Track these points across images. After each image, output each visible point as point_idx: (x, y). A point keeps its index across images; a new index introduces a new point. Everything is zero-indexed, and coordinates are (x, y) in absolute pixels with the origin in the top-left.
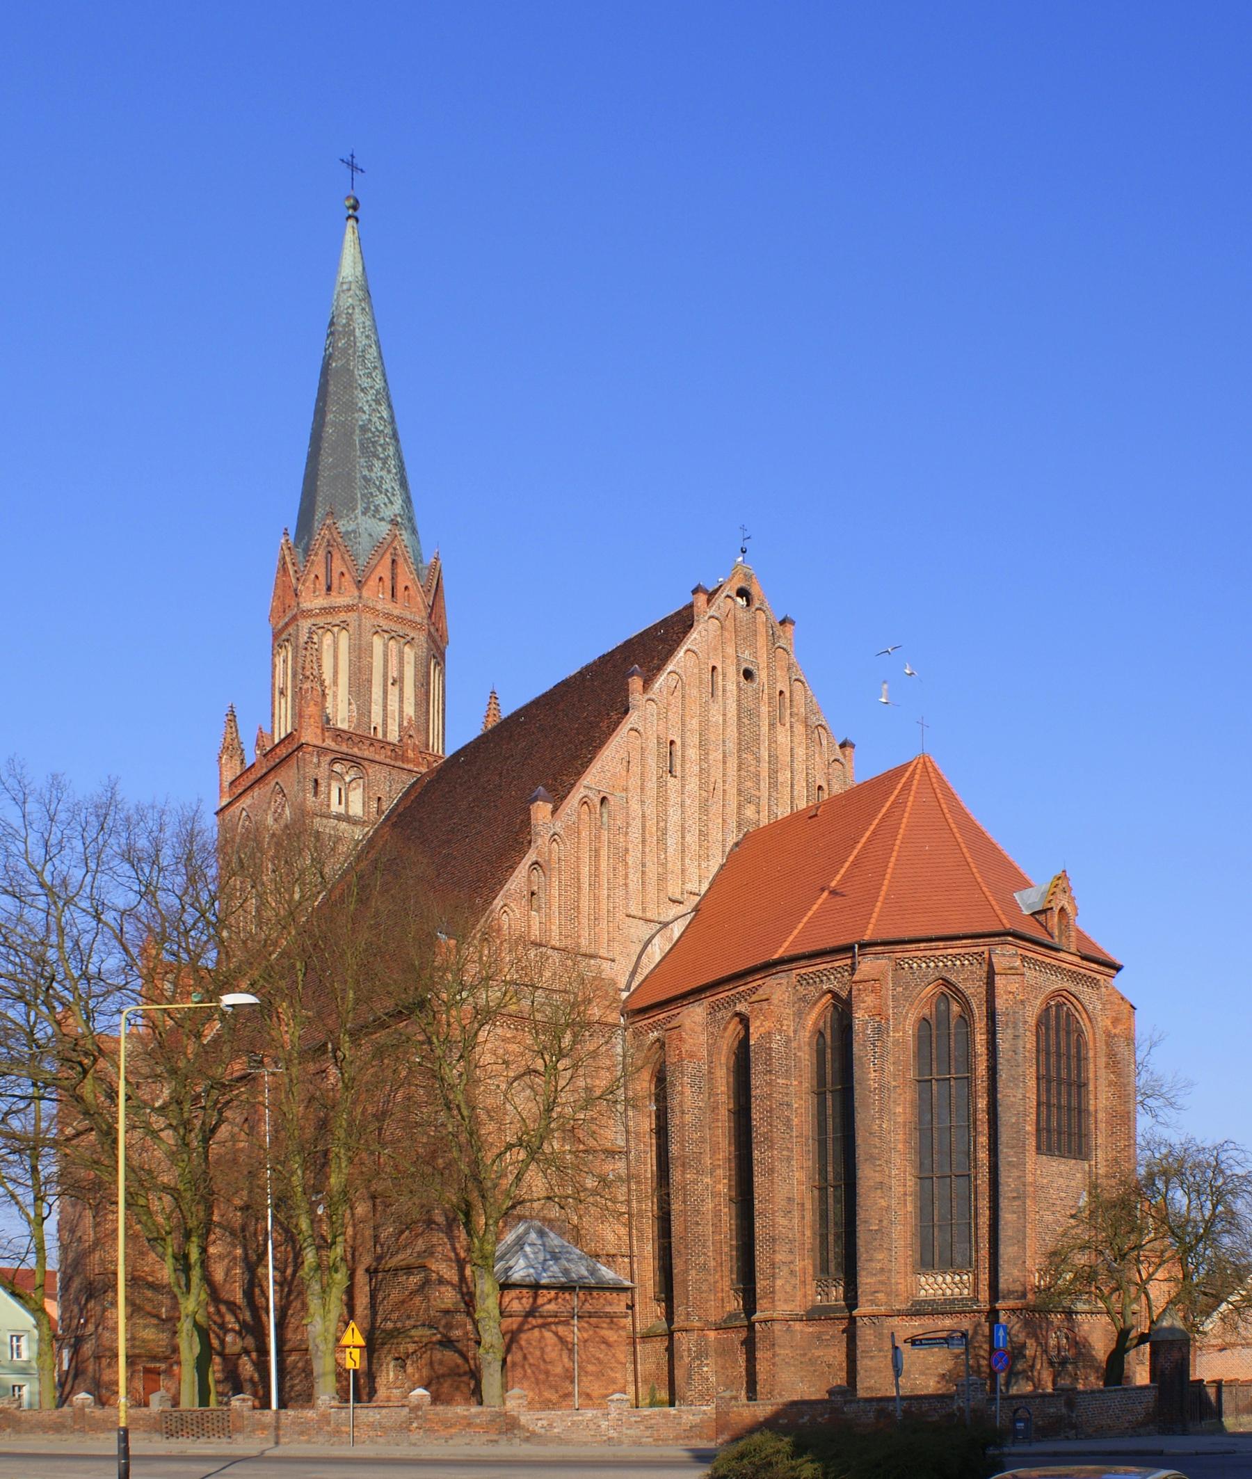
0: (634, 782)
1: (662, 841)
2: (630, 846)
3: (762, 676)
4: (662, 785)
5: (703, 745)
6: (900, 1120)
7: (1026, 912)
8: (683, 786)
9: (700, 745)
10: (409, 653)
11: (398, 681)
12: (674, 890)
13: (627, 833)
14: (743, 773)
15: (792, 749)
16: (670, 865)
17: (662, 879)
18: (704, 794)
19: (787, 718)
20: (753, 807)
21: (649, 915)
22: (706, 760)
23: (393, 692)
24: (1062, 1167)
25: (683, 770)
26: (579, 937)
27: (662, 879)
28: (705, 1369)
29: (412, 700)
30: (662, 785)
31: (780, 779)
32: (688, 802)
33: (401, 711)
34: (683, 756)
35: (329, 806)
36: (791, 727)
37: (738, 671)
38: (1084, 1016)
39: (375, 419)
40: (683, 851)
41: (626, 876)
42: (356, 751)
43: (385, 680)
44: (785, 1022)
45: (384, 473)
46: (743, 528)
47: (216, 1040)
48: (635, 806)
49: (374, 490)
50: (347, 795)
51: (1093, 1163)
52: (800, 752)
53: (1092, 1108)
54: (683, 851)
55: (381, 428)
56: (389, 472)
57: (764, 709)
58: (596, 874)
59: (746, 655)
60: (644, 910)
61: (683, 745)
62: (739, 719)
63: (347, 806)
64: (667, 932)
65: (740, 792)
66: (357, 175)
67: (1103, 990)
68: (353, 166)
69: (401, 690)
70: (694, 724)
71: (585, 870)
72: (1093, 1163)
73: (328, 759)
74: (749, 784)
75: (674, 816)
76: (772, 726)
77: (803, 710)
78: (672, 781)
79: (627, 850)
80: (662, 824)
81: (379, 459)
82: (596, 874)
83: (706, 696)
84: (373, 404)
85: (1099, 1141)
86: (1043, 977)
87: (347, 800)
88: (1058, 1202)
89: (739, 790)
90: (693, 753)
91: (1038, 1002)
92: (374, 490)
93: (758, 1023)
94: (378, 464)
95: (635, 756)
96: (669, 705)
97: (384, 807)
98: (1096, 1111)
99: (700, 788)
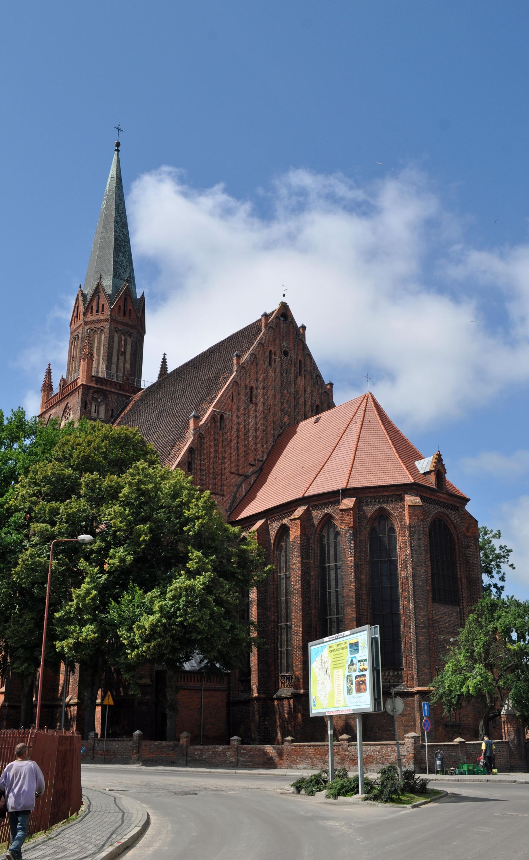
0: (235, 407)
1: (246, 435)
2: (233, 438)
3: (292, 353)
4: (247, 408)
5: (265, 388)
6: (364, 582)
7: (422, 472)
8: (256, 408)
9: (264, 388)
10: (129, 340)
11: (124, 353)
12: (251, 459)
13: (231, 432)
15: (305, 387)
17: (246, 454)
18: (266, 411)
19: (303, 372)
20: (287, 417)
21: (240, 472)
22: (267, 395)
23: (121, 359)
24: (446, 610)
25: (256, 400)
26: (209, 484)
27: (246, 454)
28: (266, 723)
29: (129, 362)
30: (247, 408)
31: (300, 402)
32: (258, 415)
33: (124, 367)
34: (256, 393)
35: (90, 414)
36: (305, 377)
37: (281, 352)
38: (452, 526)
39: (121, 235)
41: (230, 453)
42: (104, 387)
43: (118, 354)
44: (307, 530)
45: (123, 259)
46: (284, 285)
49: (119, 266)
50: (98, 408)
51: (461, 607)
52: (308, 389)
53: (459, 576)
54: (256, 440)
55: (123, 239)
56: (125, 258)
57: (292, 369)
59: (285, 344)
60: (238, 469)
61: (257, 388)
62: (282, 374)
63: (98, 414)
64: (248, 481)
65: (281, 410)
66: (121, 133)
68: (119, 130)
69: (125, 358)
70: (261, 378)
72: (461, 607)
73: (92, 391)
74: (285, 405)
75: (252, 423)
76: (296, 377)
77: (309, 368)
78: (252, 407)
79: (231, 440)
80: (247, 427)
81: (122, 252)
83: (267, 364)
85: (464, 595)
86: (431, 506)
87: (98, 410)
88: (445, 629)
89: (281, 409)
90: (260, 391)
91: (429, 519)
92: (119, 266)
93: (294, 530)
95: (235, 394)
96: (251, 369)
97: (114, 414)
98: (461, 578)
99: (264, 408)
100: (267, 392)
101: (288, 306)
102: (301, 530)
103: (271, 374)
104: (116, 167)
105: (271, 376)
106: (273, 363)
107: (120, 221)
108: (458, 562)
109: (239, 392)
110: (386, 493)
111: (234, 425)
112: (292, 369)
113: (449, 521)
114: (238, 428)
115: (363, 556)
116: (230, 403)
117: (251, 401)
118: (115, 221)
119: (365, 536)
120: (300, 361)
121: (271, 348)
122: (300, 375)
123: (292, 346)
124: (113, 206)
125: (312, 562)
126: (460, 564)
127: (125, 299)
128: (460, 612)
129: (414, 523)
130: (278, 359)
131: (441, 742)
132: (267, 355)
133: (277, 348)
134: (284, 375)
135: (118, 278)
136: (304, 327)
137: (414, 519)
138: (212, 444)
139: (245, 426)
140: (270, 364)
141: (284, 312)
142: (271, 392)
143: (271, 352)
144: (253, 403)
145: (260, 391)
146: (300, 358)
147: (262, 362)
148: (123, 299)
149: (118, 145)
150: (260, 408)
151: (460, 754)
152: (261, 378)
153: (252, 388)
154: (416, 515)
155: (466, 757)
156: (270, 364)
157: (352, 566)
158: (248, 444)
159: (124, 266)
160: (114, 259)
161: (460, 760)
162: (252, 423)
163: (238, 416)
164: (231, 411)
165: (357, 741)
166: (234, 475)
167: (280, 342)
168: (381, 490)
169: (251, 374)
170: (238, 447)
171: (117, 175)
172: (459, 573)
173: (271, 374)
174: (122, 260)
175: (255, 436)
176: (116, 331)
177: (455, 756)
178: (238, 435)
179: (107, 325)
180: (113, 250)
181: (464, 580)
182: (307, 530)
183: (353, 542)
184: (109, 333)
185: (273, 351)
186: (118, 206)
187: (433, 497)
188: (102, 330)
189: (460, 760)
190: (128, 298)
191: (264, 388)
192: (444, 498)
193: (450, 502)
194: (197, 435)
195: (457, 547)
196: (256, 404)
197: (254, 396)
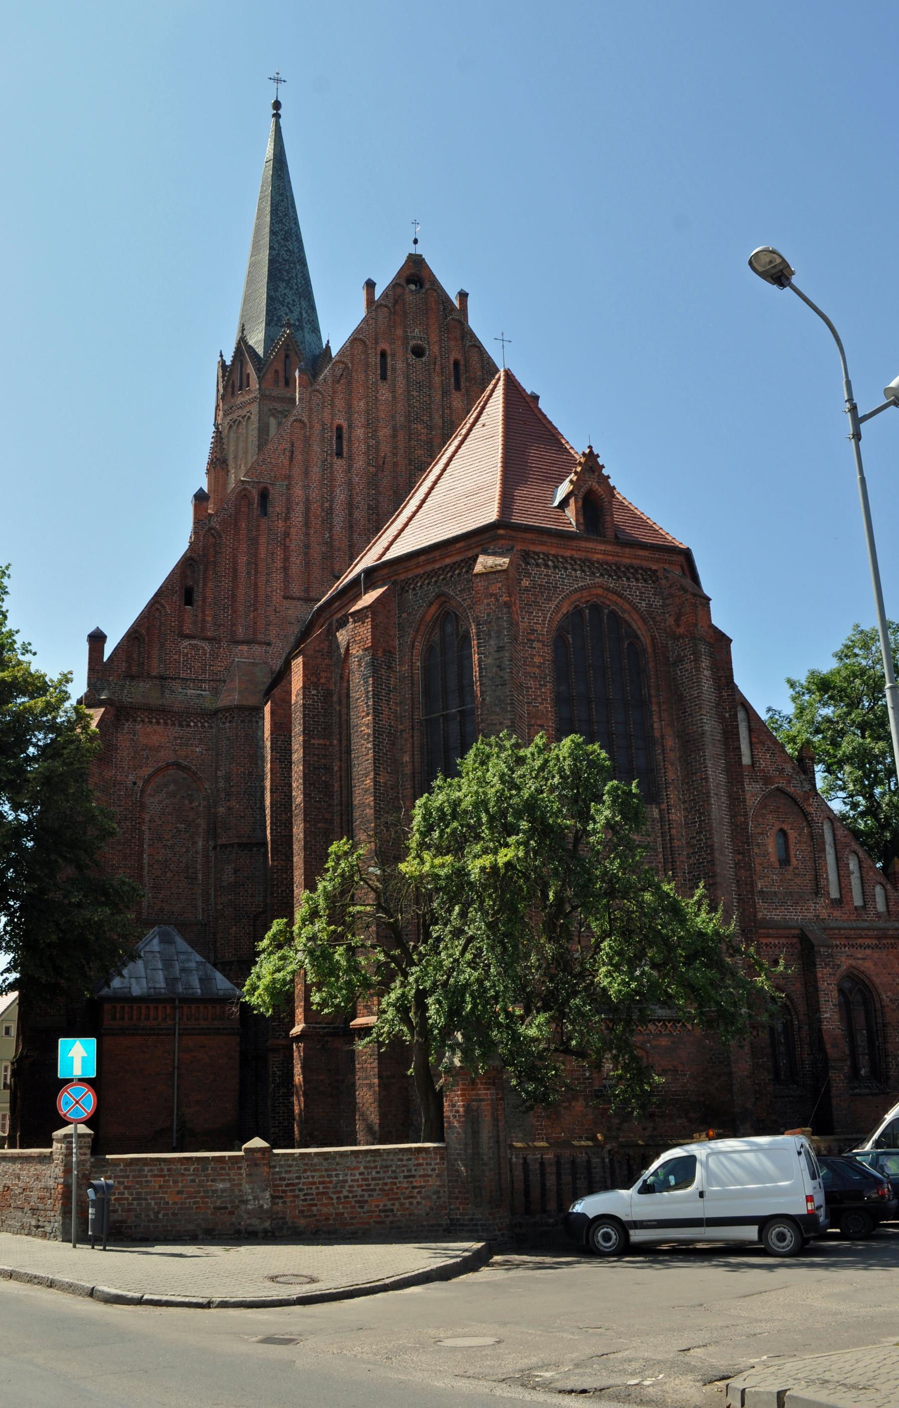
0: (297, 471)
14: (413, 443)
16: (336, 543)
25: (350, 450)
38: (636, 617)
40: (351, 527)
44: (323, 674)
47: (560, 899)
48: (298, 492)
49: (277, 305)
51: (664, 806)
53: (657, 734)
54: (351, 527)
57: (437, 379)
58: (254, 561)
61: (350, 426)
66: (281, 86)
67: (664, 581)
68: (278, 81)
70: (360, 405)
71: (243, 559)
75: (341, 496)
76: (445, 393)
77: (479, 373)
78: (339, 464)
81: (284, 281)
82: (254, 561)
84: (282, 242)
90: (359, 432)
92: (277, 305)
94: (282, 285)
95: (299, 444)
96: (334, 392)
98: (662, 737)
99: (369, 464)
100: (375, 431)
101: (424, 259)
102: (305, 675)
103: (384, 394)
104: (273, 144)
105: (386, 400)
106: (389, 373)
107: (281, 230)
108: (654, 700)
109: (307, 440)
110: (448, 561)
111: (298, 504)
112: (437, 379)
113: (626, 606)
114: (308, 509)
115: (405, 711)
116: (286, 462)
117: (339, 454)
118: (271, 231)
119: (410, 664)
120: (456, 363)
121: (383, 345)
122: (458, 387)
123: (434, 338)
124: (268, 209)
125: (335, 742)
126: (659, 704)
127: (287, 357)
128: (662, 819)
129: (488, 615)
130: (400, 365)
131: (331, 1145)
132: (375, 360)
133: (399, 343)
134: (415, 393)
135: (276, 325)
136: (463, 296)
137: (488, 605)
138: (244, 547)
139: (323, 504)
140: (384, 377)
141: (416, 273)
142: (384, 432)
143: (383, 354)
144: (342, 458)
145: (359, 432)
146: (455, 355)
147: (362, 377)
148: (282, 357)
149: (277, 105)
150: (360, 463)
151: (246, 1187)
152: (360, 405)
153: (339, 429)
154: (492, 595)
155: (267, 1195)
156: (384, 377)
157: (369, 735)
158: (330, 537)
159: (289, 303)
160: (268, 294)
161: (246, 1202)
162: (341, 496)
163: (306, 487)
164: (289, 477)
165: (21, 1148)
166: (295, 602)
167: (406, 332)
168: (437, 554)
169: (337, 402)
170: (307, 546)
171: (274, 154)
172: (656, 726)
173: (384, 394)
174: (285, 294)
175: (350, 522)
176: (273, 415)
177: (223, 1191)
178: (307, 524)
179: (254, 408)
180: (266, 280)
181: (670, 742)
182: (323, 674)
183: (371, 681)
184: (259, 420)
185: (389, 352)
186: (277, 205)
187: (568, 553)
188: (249, 417)
189: (246, 1202)
190: (292, 354)
191: (367, 425)
192: (605, 553)
193: (627, 561)
194: (202, 533)
195: (651, 665)
196: (350, 458)
197: (345, 443)
